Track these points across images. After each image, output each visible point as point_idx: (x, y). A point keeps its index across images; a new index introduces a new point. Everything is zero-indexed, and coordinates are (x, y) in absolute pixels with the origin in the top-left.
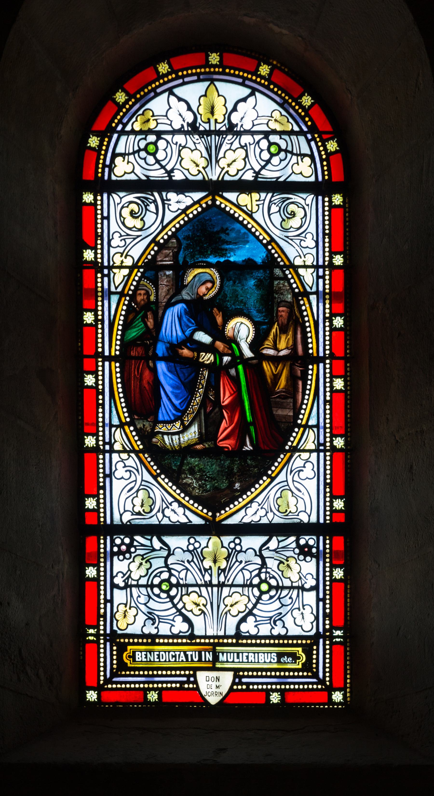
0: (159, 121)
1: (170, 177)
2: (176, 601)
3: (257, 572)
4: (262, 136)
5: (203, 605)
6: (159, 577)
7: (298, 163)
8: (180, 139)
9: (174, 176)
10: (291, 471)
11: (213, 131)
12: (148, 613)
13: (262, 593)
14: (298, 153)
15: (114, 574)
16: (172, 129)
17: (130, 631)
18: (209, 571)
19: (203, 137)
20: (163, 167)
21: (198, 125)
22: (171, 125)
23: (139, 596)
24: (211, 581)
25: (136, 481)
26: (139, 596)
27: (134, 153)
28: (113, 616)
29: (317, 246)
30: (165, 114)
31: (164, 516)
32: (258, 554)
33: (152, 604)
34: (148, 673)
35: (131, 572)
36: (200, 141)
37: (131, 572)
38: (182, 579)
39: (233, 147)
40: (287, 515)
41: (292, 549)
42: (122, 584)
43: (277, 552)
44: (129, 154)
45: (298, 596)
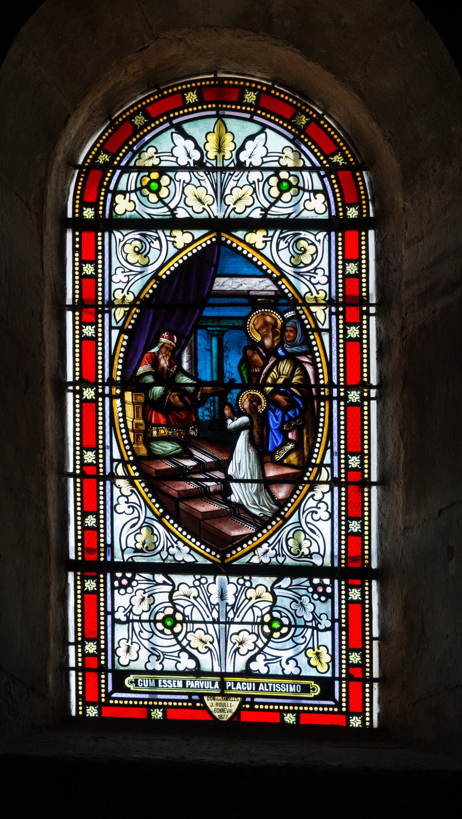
0: (162, 158)
1: (173, 215)
2: (180, 638)
3: (268, 609)
4: (272, 173)
5: (210, 642)
6: (163, 612)
7: (310, 200)
8: (183, 176)
9: (177, 214)
10: (304, 512)
11: (220, 167)
12: (152, 648)
13: (273, 630)
14: (310, 188)
15: (116, 610)
16: (178, 165)
17: (133, 666)
18: (217, 607)
19: (209, 174)
20: (166, 205)
21: (204, 161)
22: (176, 162)
23: (141, 631)
24: (218, 619)
25: (139, 517)
26: (141, 631)
27: (135, 191)
28: (114, 652)
29: (329, 281)
30: (170, 151)
31: (169, 554)
32: (269, 590)
33: (156, 640)
34: (78, 199)
35: (133, 606)
36: (205, 177)
37: (133, 606)
38: (188, 616)
39: (240, 184)
40: (300, 557)
41: (307, 588)
42: (124, 619)
43: (290, 590)
44: (131, 192)
45: (312, 634)
